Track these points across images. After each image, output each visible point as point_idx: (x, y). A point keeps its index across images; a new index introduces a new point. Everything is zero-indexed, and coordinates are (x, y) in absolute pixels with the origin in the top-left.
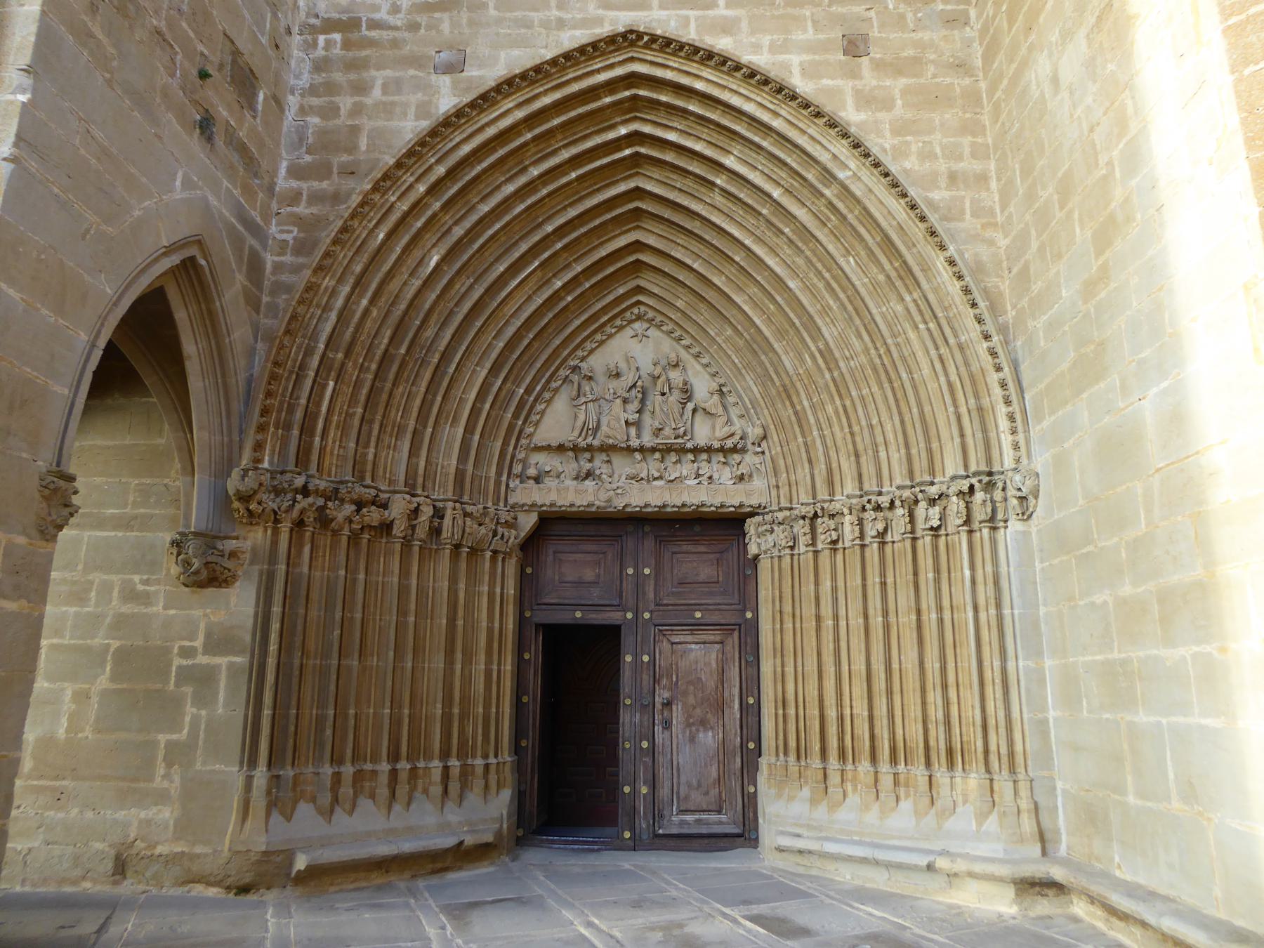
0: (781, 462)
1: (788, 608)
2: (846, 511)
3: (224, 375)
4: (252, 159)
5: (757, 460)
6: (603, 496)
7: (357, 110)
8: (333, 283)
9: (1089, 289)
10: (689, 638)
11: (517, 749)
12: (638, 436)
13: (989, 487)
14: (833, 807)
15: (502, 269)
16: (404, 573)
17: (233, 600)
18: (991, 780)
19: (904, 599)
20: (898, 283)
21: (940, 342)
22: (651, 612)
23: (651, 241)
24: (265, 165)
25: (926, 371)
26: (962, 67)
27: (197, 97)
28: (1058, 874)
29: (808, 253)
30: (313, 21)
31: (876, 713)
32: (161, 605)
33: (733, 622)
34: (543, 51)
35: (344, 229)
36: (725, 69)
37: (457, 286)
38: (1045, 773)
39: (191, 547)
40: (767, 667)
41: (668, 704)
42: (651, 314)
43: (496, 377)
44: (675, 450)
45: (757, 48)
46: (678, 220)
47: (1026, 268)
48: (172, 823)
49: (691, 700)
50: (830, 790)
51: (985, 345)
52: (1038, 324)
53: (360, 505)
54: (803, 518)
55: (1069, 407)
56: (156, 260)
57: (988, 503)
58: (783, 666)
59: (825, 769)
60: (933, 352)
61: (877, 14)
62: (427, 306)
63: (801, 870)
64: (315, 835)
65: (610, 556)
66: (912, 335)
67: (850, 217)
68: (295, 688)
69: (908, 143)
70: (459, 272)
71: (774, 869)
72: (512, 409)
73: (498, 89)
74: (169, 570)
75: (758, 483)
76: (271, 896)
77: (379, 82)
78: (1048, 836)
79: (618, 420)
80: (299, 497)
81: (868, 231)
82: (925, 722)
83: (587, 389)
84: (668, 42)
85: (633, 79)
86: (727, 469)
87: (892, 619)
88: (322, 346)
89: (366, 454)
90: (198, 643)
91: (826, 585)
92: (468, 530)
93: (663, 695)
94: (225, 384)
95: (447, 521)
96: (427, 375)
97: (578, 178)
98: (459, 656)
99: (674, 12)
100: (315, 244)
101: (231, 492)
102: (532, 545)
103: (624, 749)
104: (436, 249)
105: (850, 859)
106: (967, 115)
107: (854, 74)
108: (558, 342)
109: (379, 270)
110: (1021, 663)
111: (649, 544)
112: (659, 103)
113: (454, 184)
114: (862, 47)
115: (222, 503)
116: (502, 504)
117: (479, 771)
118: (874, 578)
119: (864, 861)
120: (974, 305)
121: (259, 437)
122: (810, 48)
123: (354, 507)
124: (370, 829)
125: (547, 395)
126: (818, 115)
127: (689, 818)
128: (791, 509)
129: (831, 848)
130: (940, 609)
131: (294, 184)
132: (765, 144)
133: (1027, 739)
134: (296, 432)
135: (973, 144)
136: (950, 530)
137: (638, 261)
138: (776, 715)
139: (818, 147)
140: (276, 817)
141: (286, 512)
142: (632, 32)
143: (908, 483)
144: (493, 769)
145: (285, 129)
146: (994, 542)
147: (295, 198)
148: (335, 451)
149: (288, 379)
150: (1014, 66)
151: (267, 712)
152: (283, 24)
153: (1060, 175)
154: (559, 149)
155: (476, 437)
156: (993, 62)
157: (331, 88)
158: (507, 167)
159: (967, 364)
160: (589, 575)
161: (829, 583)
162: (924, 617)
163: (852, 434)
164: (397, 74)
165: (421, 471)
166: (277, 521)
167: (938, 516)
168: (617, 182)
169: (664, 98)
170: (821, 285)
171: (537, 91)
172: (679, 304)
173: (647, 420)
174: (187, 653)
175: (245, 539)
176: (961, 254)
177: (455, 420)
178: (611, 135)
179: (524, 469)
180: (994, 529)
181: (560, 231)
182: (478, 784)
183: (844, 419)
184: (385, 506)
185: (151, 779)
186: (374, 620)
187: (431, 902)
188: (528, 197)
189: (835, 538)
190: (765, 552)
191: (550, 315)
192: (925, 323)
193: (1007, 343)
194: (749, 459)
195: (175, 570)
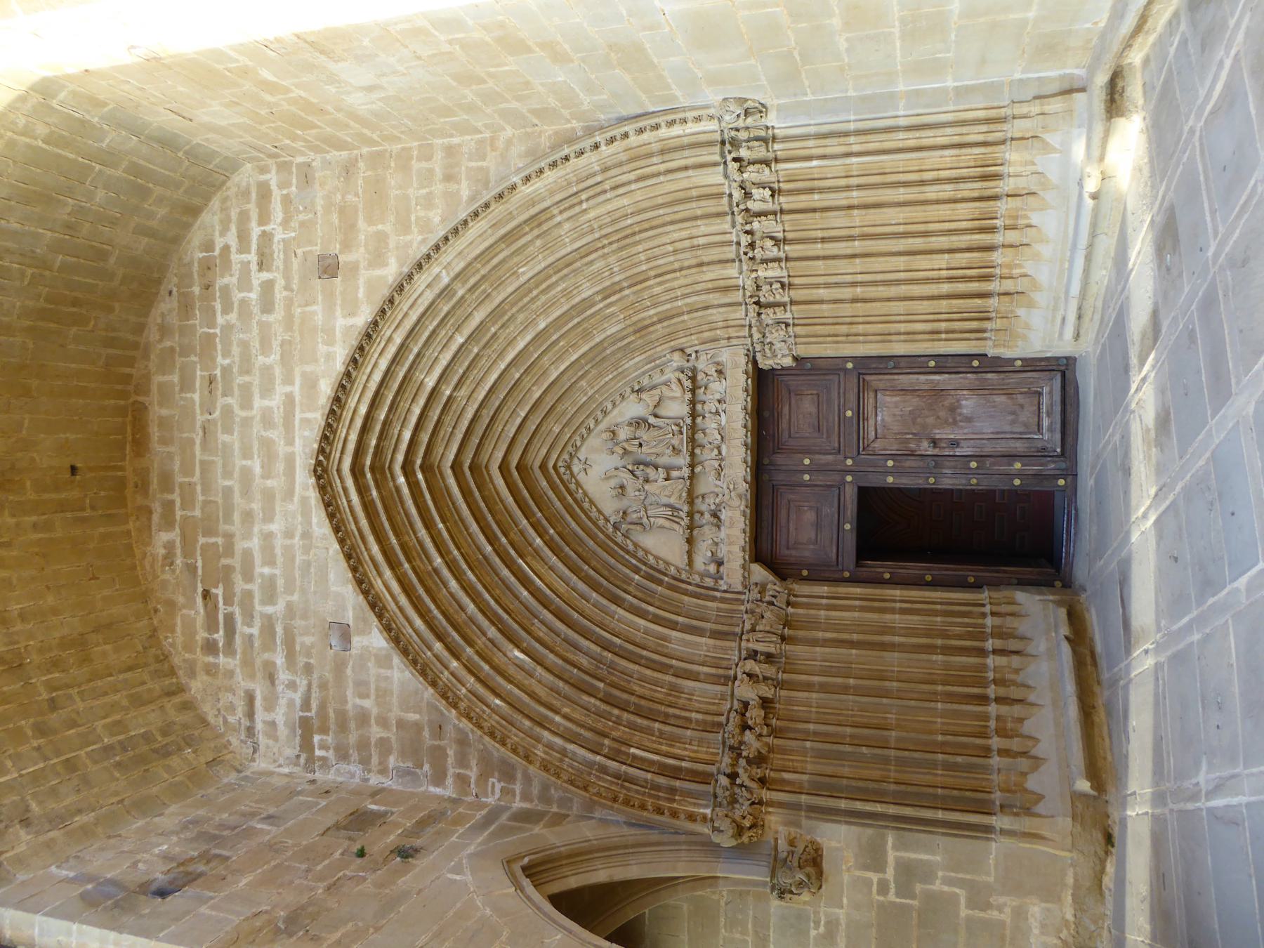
0: (706, 335)
1: (844, 329)
2: (754, 275)
3: (626, 847)
4: (429, 816)
5: (703, 358)
6: (736, 502)
7: (383, 722)
8: (540, 746)
9: (559, 57)
10: (872, 422)
11: (977, 586)
12: (680, 468)
13: (735, 143)
14: (1036, 286)
15: (526, 593)
16: (808, 687)
17: (834, 844)
18: (1012, 139)
19: (837, 221)
20: (545, 227)
21: (598, 189)
22: (846, 458)
23: (499, 455)
24: (433, 806)
25: (625, 201)
26: (348, 170)
27: (381, 860)
28: (1102, 79)
29: (514, 310)
30: (302, 760)
31: (946, 246)
32: (837, 910)
33: (856, 381)
34: (331, 552)
35: (492, 735)
36: (349, 386)
37: (541, 634)
38: (1006, 90)
39: (785, 880)
40: (900, 349)
41: (935, 443)
42: (566, 456)
43: (624, 600)
44: (693, 435)
45: (329, 357)
46: (481, 430)
47: (534, 112)
48: (1043, 905)
49: (931, 420)
50: (1020, 290)
51: (603, 148)
52: (586, 100)
53: (745, 727)
54: (759, 314)
55: (665, 73)
56: (528, 898)
57: (750, 144)
58: (900, 334)
59: (999, 294)
60: (609, 195)
61: (299, 247)
62: (560, 662)
63: (1097, 317)
64: (1057, 770)
65: (792, 497)
66: (592, 214)
67: (484, 272)
68: (914, 789)
69: (417, 218)
70: (529, 633)
71: (1097, 340)
72: (654, 586)
73: (366, 593)
74: (805, 903)
75: (725, 356)
76: (1115, 815)
77: (358, 701)
78: (1066, 86)
79: (665, 487)
80: (738, 781)
81: (497, 255)
82: (956, 201)
83: (635, 516)
84: (325, 438)
85: (356, 471)
86: (711, 385)
87: (856, 232)
88: (598, 758)
89: (697, 721)
90: (874, 877)
91: (823, 293)
92: (768, 628)
93: (925, 448)
94: (633, 846)
95: (760, 647)
96: (624, 663)
97: (444, 522)
98: (887, 638)
99: (297, 433)
100: (504, 762)
101: (733, 843)
102: (781, 570)
103: (977, 485)
104: (509, 654)
105: (1087, 272)
106: (393, 164)
107: (354, 268)
108: (592, 543)
109: (528, 705)
110: (901, 113)
111: (780, 459)
112: (377, 446)
113: (449, 635)
114: (330, 261)
115: (743, 852)
116: (743, 597)
117: (997, 621)
118: (818, 249)
119: (1088, 258)
120: (567, 158)
121: (682, 816)
122: (330, 309)
123: (747, 732)
124: (1052, 723)
125: (640, 554)
126: (391, 301)
127: (1046, 422)
128: (750, 326)
129: (1075, 289)
130: (848, 188)
131: (449, 781)
132: (416, 350)
133: (974, 106)
134: (678, 783)
135: (419, 160)
136: (774, 179)
137: (517, 468)
138: (946, 340)
139: (420, 301)
140: (1040, 808)
141: (752, 793)
142: (315, 471)
143: (729, 218)
144: (995, 609)
145: (400, 788)
146: (787, 139)
147: (462, 780)
148: (693, 749)
149: (628, 789)
150: (352, 123)
151: (940, 815)
152: (307, 787)
153: (455, 84)
154: (417, 538)
155: (680, 619)
156: (346, 141)
157: (363, 745)
158: (433, 587)
159: (620, 164)
160: (810, 516)
161: (821, 291)
162: (856, 202)
163: (681, 269)
164: (351, 684)
165: (713, 671)
166: (761, 803)
167: (761, 190)
168: (446, 486)
169: (374, 442)
170: (543, 298)
171: (367, 558)
172: (557, 429)
173: (662, 460)
174: (883, 888)
175: (777, 832)
176: (518, 170)
177: (664, 638)
178: (405, 490)
179: (710, 576)
180: (774, 138)
181: (491, 540)
182: (1010, 622)
183: (668, 277)
184: (746, 705)
185: (1003, 923)
186: (852, 716)
187: (1122, 665)
188: (460, 567)
189: (778, 285)
190: (790, 350)
191: (567, 549)
192: (581, 202)
193: (602, 128)
194: (701, 365)
195: (806, 896)
